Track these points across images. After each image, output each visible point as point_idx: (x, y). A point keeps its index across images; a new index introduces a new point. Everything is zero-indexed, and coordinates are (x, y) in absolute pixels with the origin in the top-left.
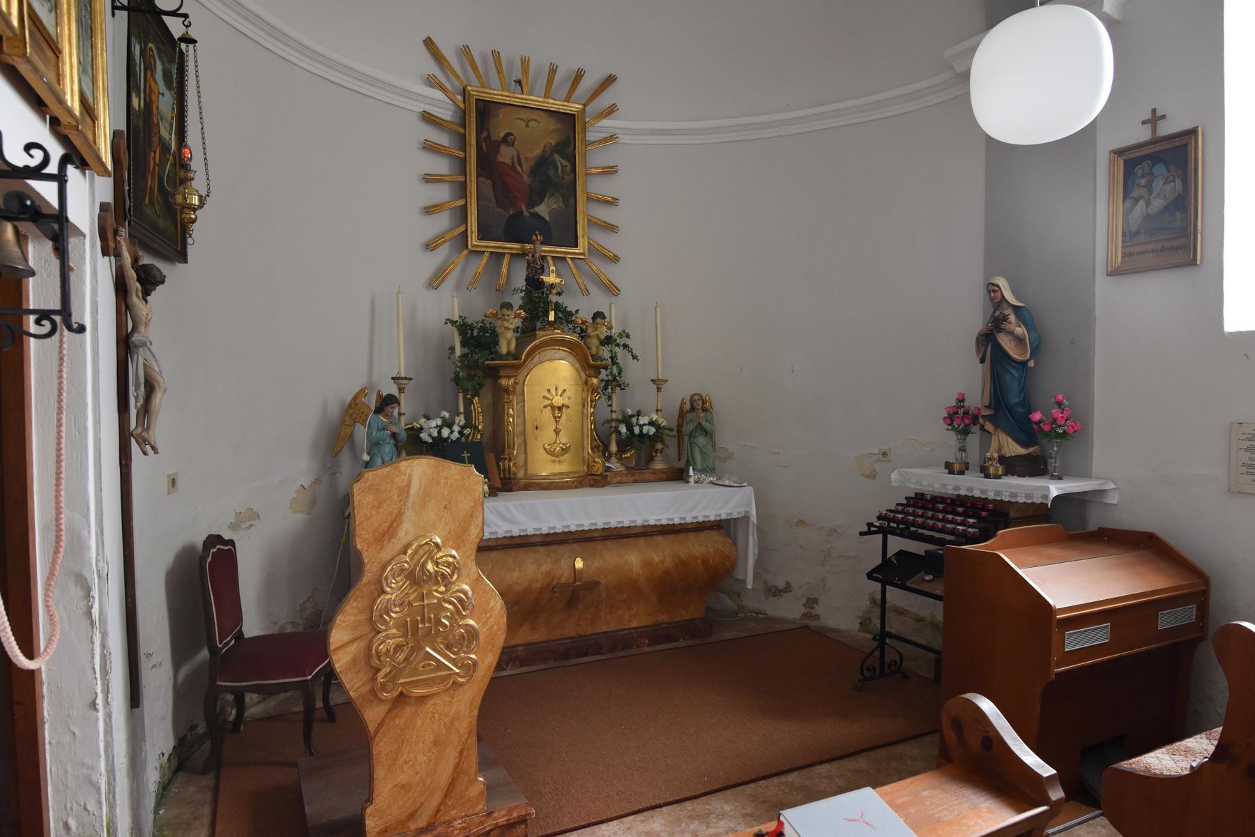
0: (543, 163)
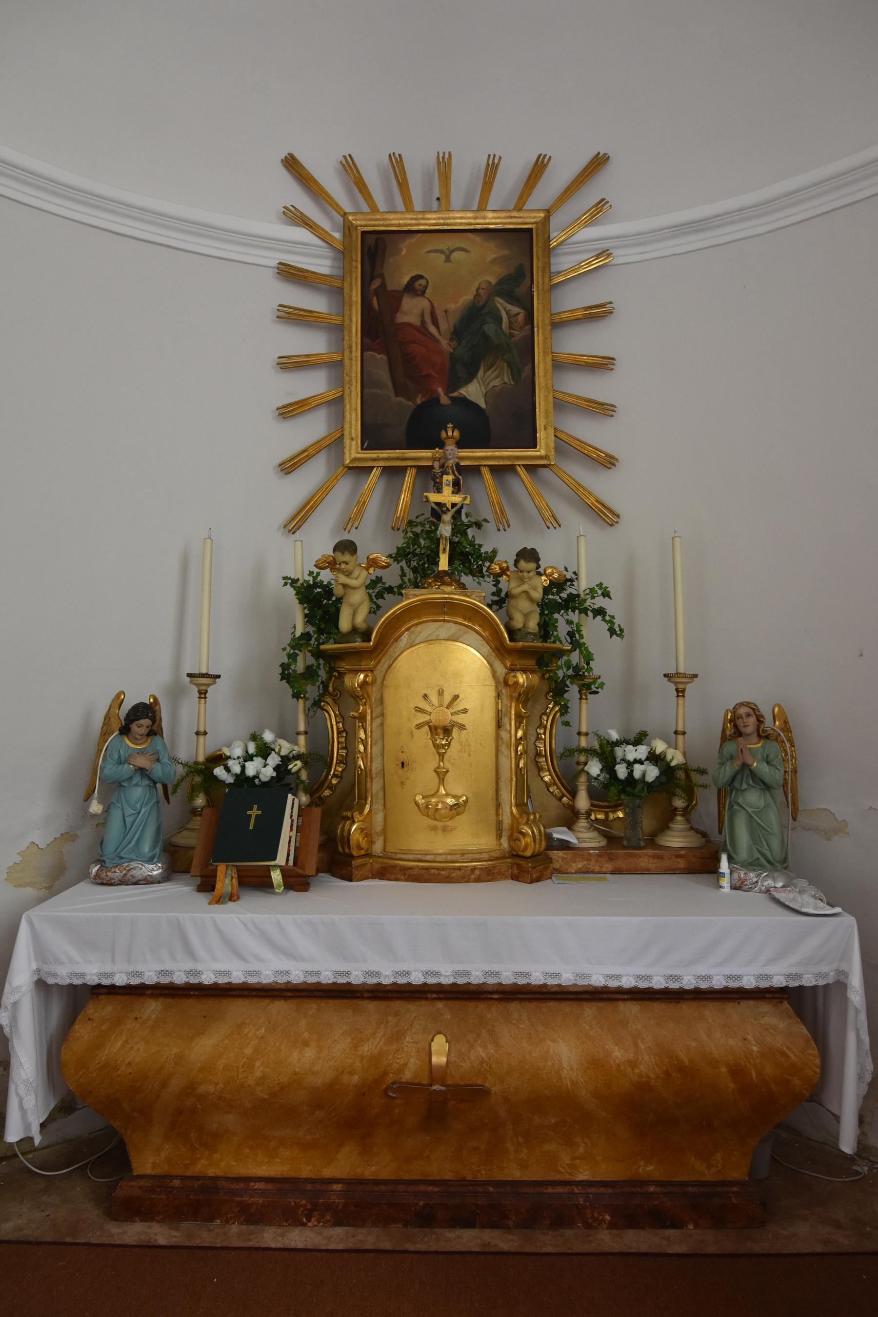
0: (476, 315)
